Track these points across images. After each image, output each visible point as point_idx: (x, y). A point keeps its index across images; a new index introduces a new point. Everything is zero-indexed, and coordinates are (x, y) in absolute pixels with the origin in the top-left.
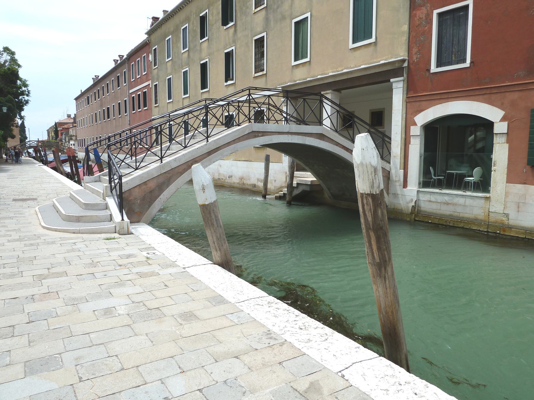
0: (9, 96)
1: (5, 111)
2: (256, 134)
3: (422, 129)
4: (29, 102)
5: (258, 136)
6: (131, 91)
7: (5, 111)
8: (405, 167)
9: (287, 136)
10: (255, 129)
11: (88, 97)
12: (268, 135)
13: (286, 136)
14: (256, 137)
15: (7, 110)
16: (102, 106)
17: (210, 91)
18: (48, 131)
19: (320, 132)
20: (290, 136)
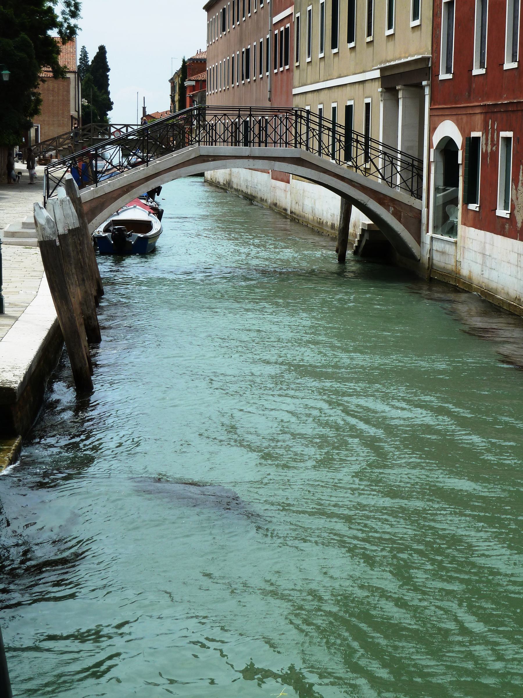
0: (23, 35)
1: (6, 78)
2: (206, 159)
3: (438, 154)
4: (78, 31)
5: (208, 161)
6: (276, 19)
7: (6, 78)
8: (428, 207)
9: (247, 160)
10: (203, 153)
11: (224, 10)
12: (221, 160)
13: (261, 161)
14: (204, 161)
15: (10, 76)
16: (241, 42)
17: (357, 48)
18: (172, 81)
19: (297, 155)
20: (251, 160)
